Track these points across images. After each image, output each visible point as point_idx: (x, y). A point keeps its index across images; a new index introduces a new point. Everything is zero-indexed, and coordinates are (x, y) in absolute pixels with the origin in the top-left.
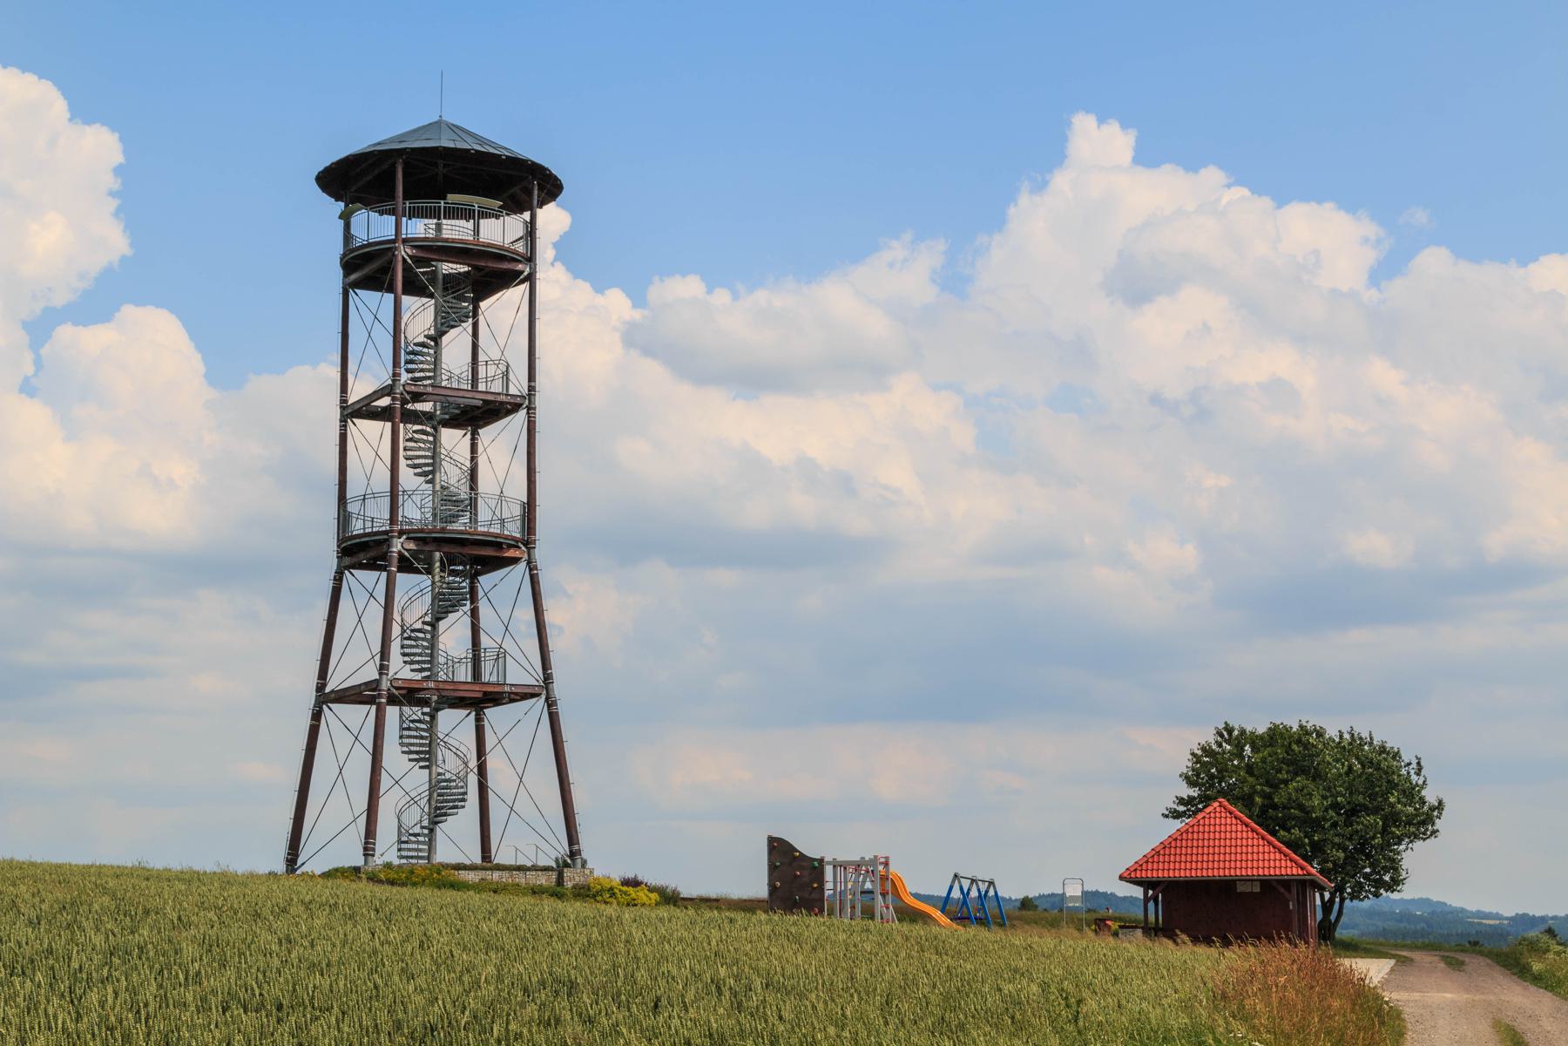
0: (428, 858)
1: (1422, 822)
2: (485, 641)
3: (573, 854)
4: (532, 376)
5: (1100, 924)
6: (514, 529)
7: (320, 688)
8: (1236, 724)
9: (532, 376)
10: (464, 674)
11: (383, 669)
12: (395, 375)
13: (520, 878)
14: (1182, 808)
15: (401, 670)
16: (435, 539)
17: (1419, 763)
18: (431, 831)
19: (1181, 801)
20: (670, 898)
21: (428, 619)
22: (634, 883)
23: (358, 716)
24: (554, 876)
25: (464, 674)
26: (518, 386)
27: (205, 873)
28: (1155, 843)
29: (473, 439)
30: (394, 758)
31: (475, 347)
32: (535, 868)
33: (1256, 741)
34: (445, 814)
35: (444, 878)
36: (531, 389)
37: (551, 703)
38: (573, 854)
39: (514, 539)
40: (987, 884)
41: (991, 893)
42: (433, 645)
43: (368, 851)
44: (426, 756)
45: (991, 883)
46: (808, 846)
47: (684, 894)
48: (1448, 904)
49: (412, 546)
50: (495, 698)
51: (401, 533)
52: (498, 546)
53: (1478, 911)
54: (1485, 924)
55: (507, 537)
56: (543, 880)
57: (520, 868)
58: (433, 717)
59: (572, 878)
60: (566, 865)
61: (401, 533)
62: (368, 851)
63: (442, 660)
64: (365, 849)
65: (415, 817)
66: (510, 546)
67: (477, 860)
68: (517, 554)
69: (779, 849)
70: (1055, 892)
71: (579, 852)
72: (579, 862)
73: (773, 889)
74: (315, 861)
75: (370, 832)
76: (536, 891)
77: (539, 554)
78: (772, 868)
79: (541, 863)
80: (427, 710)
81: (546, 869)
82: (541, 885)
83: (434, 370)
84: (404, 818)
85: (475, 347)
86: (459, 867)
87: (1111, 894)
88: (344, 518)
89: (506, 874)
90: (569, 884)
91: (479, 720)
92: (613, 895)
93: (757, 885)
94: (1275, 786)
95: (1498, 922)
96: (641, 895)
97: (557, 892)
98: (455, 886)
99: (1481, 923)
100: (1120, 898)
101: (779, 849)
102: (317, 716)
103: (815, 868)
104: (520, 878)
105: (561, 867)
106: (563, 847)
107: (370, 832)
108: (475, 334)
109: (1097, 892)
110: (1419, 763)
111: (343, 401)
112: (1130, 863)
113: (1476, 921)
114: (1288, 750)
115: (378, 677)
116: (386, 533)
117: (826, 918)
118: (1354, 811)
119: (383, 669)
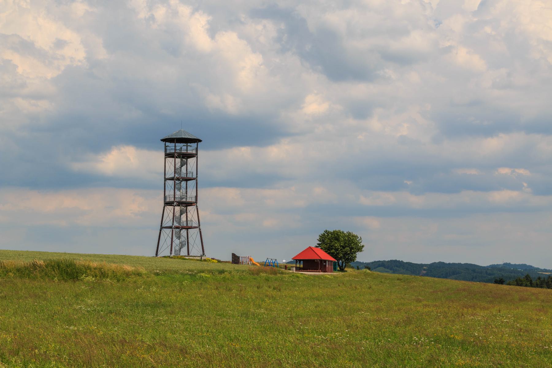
0: (180, 254)
1: (360, 249)
2: (188, 219)
3: (203, 254)
4: (197, 175)
5: (197, 260)
6: (194, 200)
7: (161, 226)
8: (327, 230)
9: (197, 175)
10: (185, 225)
11: (173, 224)
12: (175, 175)
13: (195, 258)
14: (318, 246)
15: (176, 224)
16: (181, 203)
17: (361, 238)
18: (180, 250)
19: (318, 244)
20: (219, 261)
21: (180, 167)
22: (213, 259)
23: (169, 231)
24: (200, 258)
25: (185, 225)
26: (195, 176)
27: (546, 288)
28: (298, 254)
29: (186, 183)
30: (174, 238)
31: (187, 169)
32: (197, 256)
33: (331, 233)
34: (182, 247)
35: (182, 258)
36: (197, 177)
37: (200, 229)
38: (203, 254)
39: (194, 202)
40: (275, 260)
41: (276, 262)
42: (181, 171)
43: (171, 253)
44: (179, 238)
45: (276, 260)
46: (237, 255)
47: (222, 261)
48: (533, 266)
49: (177, 204)
50: (191, 228)
51: (176, 202)
52: (191, 203)
53: (545, 269)
54: (544, 274)
55: (193, 202)
56: (199, 258)
57: (195, 256)
58: (180, 231)
59: (203, 258)
60: (202, 256)
61: (176, 202)
62: (171, 253)
63: (182, 222)
64: (171, 253)
65: (177, 248)
66: (193, 203)
67: (187, 255)
68: (194, 204)
69: (233, 255)
70: (380, 260)
71: (204, 254)
72: (204, 256)
73: (232, 260)
74: (161, 254)
75: (171, 250)
76: (197, 260)
77: (198, 204)
78: (232, 257)
79: (198, 256)
80: (180, 181)
81: (199, 256)
82: (40, 264)
83: (180, 222)
84: (176, 248)
85: (187, 169)
86: (185, 256)
87: (401, 261)
88: (165, 198)
89: (193, 257)
90: (203, 259)
91: (187, 231)
92: (210, 261)
93: (230, 259)
94: (331, 242)
95: (550, 273)
96: (214, 261)
97: (201, 260)
98: (185, 259)
99: (542, 274)
100: (405, 263)
101: (233, 255)
102: (161, 231)
103: (238, 258)
104: (195, 258)
105: (201, 256)
106: (202, 253)
107: (171, 250)
108: (187, 167)
109: (396, 260)
110: (361, 238)
111: (165, 177)
112: (294, 257)
113: (540, 273)
114: (335, 236)
115: (172, 225)
116: (173, 201)
117: (242, 265)
118: (344, 247)
119: (173, 224)
